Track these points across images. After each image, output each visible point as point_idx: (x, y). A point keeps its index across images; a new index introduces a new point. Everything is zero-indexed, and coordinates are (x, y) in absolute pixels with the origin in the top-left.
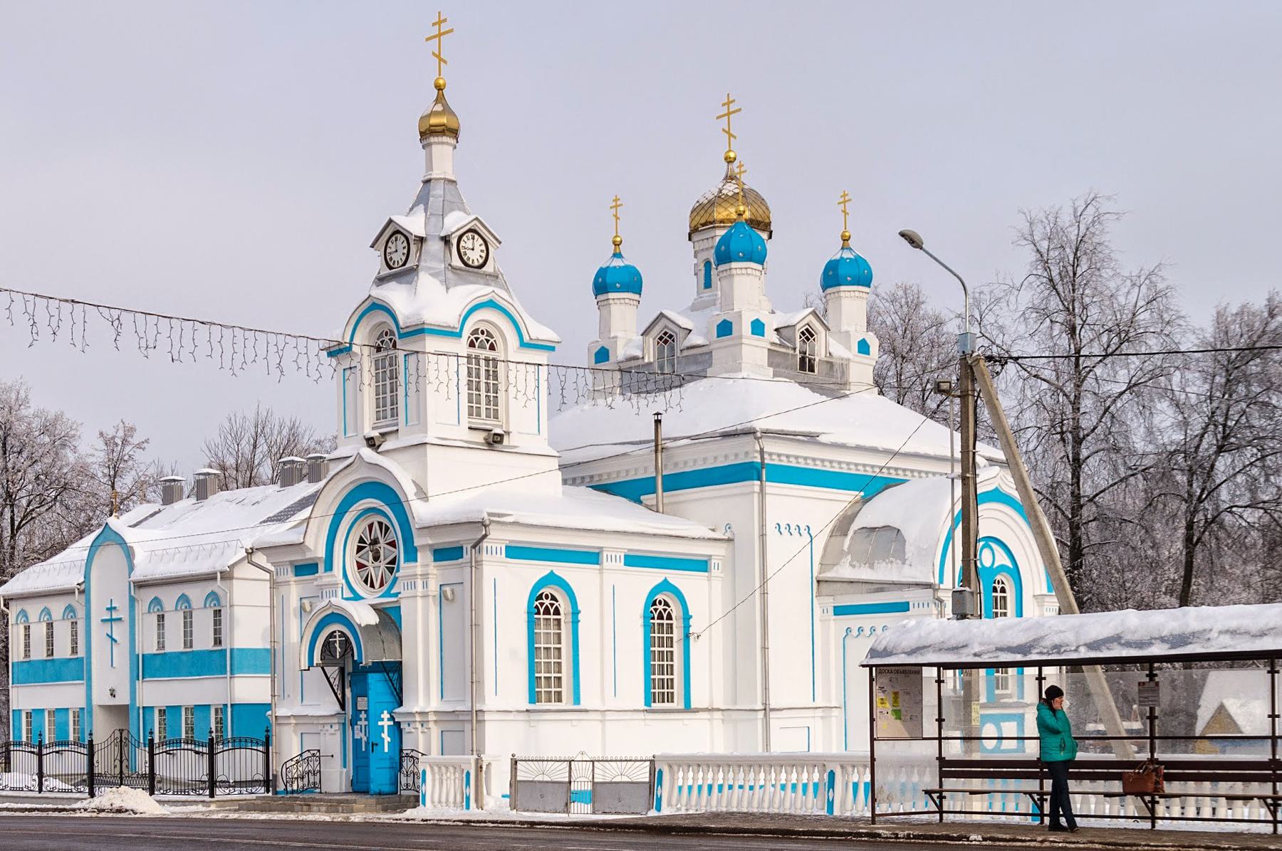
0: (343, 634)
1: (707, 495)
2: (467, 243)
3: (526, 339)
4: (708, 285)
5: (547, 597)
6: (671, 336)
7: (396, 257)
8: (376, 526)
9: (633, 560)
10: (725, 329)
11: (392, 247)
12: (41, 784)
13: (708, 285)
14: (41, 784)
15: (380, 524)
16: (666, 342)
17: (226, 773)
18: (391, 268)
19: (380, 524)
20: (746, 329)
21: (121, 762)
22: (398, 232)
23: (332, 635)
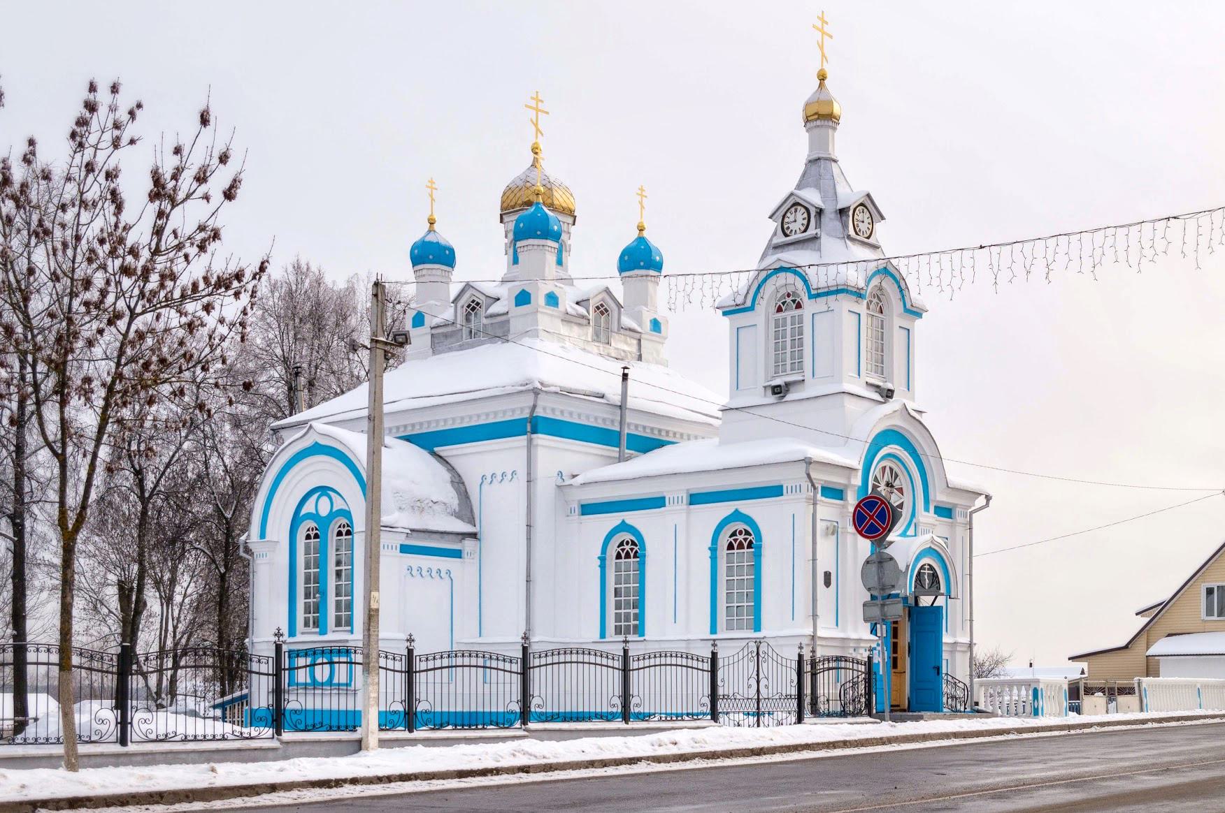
0: (931, 568)
1: (575, 448)
2: (859, 216)
3: (908, 306)
4: (516, 261)
5: (741, 533)
6: (478, 304)
7: (793, 227)
8: (888, 470)
9: (696, 499)
10: (523, 298)
11: (790, 217)
12: (124, 724)
13: (516, 261)
14: (124, 724)
15: (891, 469)
16: (602, 313)
17: (431, 699)
18: (786, 235)
19: (891, 469)
20: (542, 301)
21: (758, 682)
22: (797, 204)
23: (922, 568)
